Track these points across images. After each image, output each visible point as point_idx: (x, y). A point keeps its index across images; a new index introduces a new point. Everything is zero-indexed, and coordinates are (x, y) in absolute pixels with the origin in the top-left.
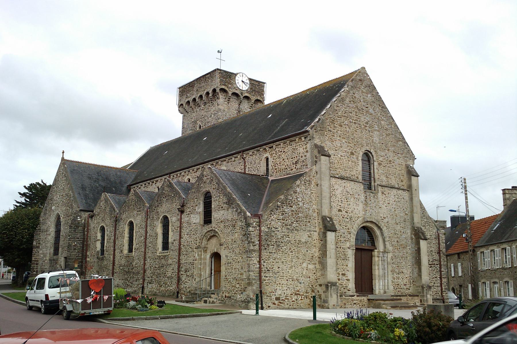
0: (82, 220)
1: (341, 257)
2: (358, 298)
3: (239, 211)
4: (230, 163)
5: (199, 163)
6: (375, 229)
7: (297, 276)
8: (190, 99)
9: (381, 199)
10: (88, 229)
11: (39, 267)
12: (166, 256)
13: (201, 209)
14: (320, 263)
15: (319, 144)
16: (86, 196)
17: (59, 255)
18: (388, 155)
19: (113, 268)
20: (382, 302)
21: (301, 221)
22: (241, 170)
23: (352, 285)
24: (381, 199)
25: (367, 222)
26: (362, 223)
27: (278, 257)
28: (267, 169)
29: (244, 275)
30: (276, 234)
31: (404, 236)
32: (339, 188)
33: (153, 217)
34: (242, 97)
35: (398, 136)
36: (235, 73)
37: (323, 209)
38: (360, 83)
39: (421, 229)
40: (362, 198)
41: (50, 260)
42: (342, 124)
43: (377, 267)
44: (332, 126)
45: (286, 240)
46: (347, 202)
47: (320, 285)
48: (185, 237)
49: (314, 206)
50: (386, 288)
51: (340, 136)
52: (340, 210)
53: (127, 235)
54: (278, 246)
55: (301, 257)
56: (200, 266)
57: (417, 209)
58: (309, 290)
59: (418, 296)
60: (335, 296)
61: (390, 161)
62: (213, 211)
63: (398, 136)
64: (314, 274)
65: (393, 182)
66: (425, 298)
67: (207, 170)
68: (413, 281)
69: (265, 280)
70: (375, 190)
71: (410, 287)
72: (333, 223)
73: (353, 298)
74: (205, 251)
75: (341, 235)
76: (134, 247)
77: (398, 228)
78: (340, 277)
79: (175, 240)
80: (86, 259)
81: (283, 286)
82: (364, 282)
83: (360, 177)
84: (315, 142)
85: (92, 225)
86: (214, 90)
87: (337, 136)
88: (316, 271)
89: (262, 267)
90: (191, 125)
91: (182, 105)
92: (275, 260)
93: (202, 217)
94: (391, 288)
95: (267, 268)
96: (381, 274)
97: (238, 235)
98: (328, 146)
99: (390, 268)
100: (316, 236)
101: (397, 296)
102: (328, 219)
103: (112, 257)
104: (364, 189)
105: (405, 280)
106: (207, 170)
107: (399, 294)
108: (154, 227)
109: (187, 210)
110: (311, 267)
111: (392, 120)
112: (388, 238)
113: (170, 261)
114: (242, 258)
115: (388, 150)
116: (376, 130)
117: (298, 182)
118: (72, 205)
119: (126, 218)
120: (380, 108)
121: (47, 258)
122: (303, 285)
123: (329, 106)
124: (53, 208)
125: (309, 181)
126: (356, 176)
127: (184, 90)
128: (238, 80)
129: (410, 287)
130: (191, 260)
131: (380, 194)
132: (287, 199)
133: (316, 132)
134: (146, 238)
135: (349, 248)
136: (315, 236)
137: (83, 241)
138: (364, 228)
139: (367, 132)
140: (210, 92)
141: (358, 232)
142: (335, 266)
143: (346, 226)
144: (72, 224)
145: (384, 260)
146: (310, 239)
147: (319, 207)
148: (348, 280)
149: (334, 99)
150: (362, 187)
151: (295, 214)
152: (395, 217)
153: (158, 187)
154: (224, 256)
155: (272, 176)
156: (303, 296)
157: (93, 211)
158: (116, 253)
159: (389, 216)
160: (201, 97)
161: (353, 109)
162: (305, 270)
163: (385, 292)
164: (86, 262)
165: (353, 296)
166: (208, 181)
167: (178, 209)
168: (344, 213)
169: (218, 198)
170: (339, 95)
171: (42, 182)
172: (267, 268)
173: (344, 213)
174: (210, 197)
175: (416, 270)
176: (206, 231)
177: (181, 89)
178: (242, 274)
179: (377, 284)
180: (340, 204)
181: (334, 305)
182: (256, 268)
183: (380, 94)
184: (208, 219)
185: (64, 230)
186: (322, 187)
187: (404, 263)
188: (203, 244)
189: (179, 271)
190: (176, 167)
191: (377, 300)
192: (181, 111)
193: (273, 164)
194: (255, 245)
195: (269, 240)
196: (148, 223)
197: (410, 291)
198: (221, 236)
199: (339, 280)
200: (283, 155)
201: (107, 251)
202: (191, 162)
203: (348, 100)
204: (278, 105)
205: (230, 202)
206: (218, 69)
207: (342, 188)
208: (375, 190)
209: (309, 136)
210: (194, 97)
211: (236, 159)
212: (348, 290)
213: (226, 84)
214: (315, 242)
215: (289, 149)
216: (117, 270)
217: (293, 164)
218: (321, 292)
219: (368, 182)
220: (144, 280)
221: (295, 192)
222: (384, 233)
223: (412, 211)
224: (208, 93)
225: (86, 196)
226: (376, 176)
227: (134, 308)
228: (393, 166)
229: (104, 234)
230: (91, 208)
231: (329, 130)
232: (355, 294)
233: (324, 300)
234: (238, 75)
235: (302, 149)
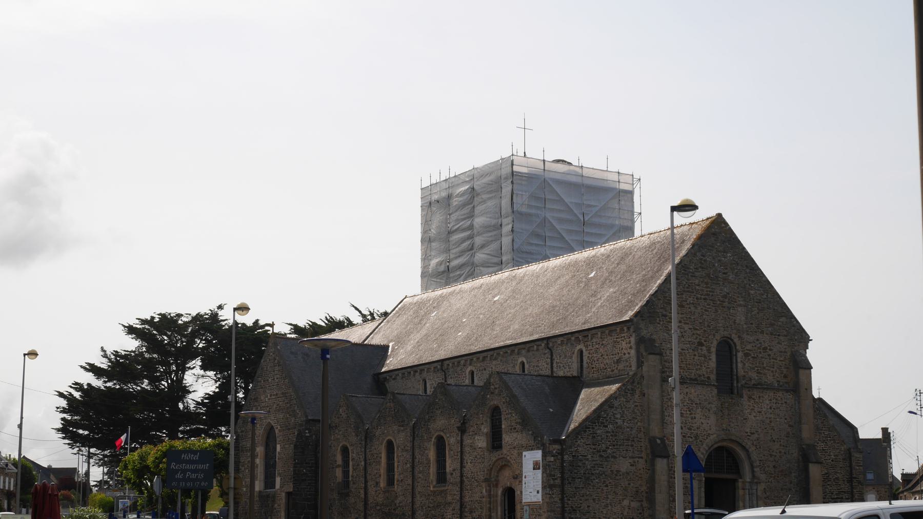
4: (531, 353)
13: (486, 429)
28: (582, 366)
42: (684, 303)
48: (468, 466)
49: (639, 424)
61: (765, 349)
74: (497, 486)
79: (454, 470)
83: (713, 377)
100: (641, 464)
103: (362, 492)
113: (449, 498)
116: (740, 305)
125: (632, 390)
134: (413, 467)
138: (720, 449)
150: (715, 391)
159: (759, 430)
162: (627, 510)
166: (497, 391)
176: (495, 459)
184: (496, 442)
196: (416, 443)
228: (769, 355)
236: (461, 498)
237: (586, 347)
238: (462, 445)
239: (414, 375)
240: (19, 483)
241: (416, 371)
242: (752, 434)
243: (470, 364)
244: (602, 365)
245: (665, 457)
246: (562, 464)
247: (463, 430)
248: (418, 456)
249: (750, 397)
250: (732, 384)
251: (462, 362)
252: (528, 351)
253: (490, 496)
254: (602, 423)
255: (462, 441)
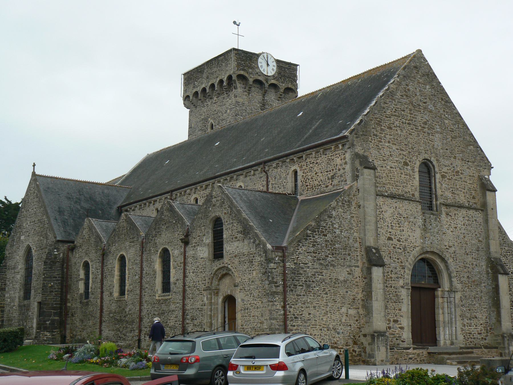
0: (59, 254)
1: (391, 298)
2: (415, 351)
3: (257, 242)
4: (248, 178)
5: (209, 177)
6: (438, 261)
7: (334, 324)
8: (199, 89)
9: (445, 222)
10: (68, 265)
11: (5, 316)
12: (167, 300)
13: (208, 239)
14: (364, 306)
15: (361, 152)
16: (64, 222)
17: (32, 298)
18: (454, 165)
19: (101, 316)
20: (447, 356)
21: (338, 254)
22: (263, 186)
23: (407, 335)
24: (445, 222)
25: (427, 252)
26: (421, 255)
27: (309, 300)
28: (296, 186)
29: (265, 324)
30: (305, 271)
31: (477, 270)
32: (388, 209)
33: (150, 250)
34: (267, 85)
35: (468, 138)
36: (257, 53)
37: (367, 237)
38: (415, 71)
39: (501, 261)
40: (420, 221)
41: (20, 306)
43: (441, 311)
44: (379, 129)
45: (318, 279)
46: (400, 227)
47: (365, 336)
48: (191, 275)
49: (355, 234)
50: (454, 337)
51: (389, 142)
52: (390, 239)
53: (117, 273)
54: (308, 286)
55: (338, 299)
56: (209, 313)
57: (494, 234)
58: (350, 342)
59: (497, 348)
60: (383, 349)
61: (457, 172)
62: (224, 242)
63: (468, 138)
64: (357, 321)
65: (462, 199)
66: (507, 351)
67: (216, 189)
68: (491, 329)
69: (292, 330)
70: (437, 211)
71: (487, 336)
72: (380, 255)
73: (408, 351)
75: (392, 271)
76: (126, 288)
77: (469, 259)
78: (391, 325)
79: (177, 280)
80: (66, 304)
81: (316, 337)
82: (425, 331)
83: (417, 194)
84: (356, 150)
85: (73, 260)
86: (230, 78)
87: (385, 142)
88: (360, 317)
89: (288, 313)
90: (200, 124)
91: (188, 97)
92: (304, 304)
93: (212, 249)
94: (461, 337)
95: (294, 315)
96: (447, 319)
97: (256, 274)
98: (373, 156)
99: (459, 313)
100: (358, 272)
101: (468, 348)
102: (374, 251)
103: (99, 301)
104: (422, 209)
105: (480, 328)
106: (216, 189)
107: (472, 346)
108: (151, 263)
109: (193, 241)
110: (352, 312)
111: (458, 118)
112: (455, 273)
113: (172, 307)
114: (262, 302)
115: (455, 158)
116: (437, 132)
117: (334, 204)
118: (46, 234)
119: (117, 250)
120: (443, 103)
121: (16, 304)
122: (342, 335)
123: (373, 103)
124: (22, 238)
125: (349, 201)
126: (411, 193)
127: (190, 77)
128: (261, 63)
129: (487, 336)
130: (198, 305)
131: (444, 216)
132: (319, 226)
133: (357, 137)
134: (141, 278)
135: (402, 287)
136: (357, 273)
137: (62, 281)
138: (423, 260)
139: (426, 134)
140: (225, 79)
141: (414, 266)
142: (383, 310)
143: (398, 259)
144: (46, 259)
145: (450, 302)
146: (351, 276)
147: (362, 235)
148: (402, 328)
149: (381, 94)
150: (420, 207)
151: (331, 244)
152: (464, 245)
153: (157, 209)
154: (240, 300)
155: (301, 194)
156: (342, 350)
157: (73, 242)
158: (104, 297)
159: (456, 244)
160: (213, 86)
161: (406, 106)
163: (452, 343)
164: (66, 307)
165: (408, 349)
167: (181, 240)
168: (395, 241)
169: (231, 226)
170: (387, 88)
171: (6, 199)
172: (294, 315)
173: (395, 241)
174: (221, 224)
175: (494, 315)
176: (216, 268)
177: (186, 76)
178: (262, 323)
179: (442, 333)
180: (391, 230)
181: (382, 361)
182: (280, 315)
183: (443, 84)
184: (218, 252)
185: (37, 267)
186: (366, 209)
187: (477, 305)
188: (213, 285)
189: (184, 319)
190: (180, 183)
191: (440, 353)
192: (187, 104)
193: (303, 180)
194: (278, 286)
195: (297, 278)
196: (145, 257)
197: (487, 341)
198: (236, 274)
199: (390, 328)
200: (315, 168)
201: (92, 294)
202: (199, 176)
203: (399, 94)
204: (312, 97)
205: (246, 231)
206: (234, 49)
207: (392, 210)
208: (437, 211)
209: (347, 143)
210: (203, 86)
211: (257, 172)
212: (403, 341)
213: (246, 68)
214: (357, 280)
215: (323, 159)
216: (105, 318)
217: (329, 179)
218: (366, 344)
219: (429, 202)
220: (140, 331)
221: (330, 217)
222: (450, 266)
223: (487, 237)
224: (221, 81)
225: (64, 222)
226: (439, 192)
227: (126, 366)
228: (461, 178)
229: (89, 272)
230: (71, 238)
231: (374, 135)
232: (412, 346)
233: (369, 354)
234: (261, 56)
235: (341, 160)
236: (184, 305)
237: (301, 167)
238: (185, 256)
239: (149, 206)
240: (227, 315)
241: (150, 203)
242: (450, 247)
243: (195, 193)
244: (316, 183)
245: (381, 266)
246: (284, 271)
247: (186, 242)
248: (146, 269)
249: (447, 214)
250: (431, 202)
251: (188, 191)
252: (246, 176)
253: (211, 304)
254: (322, 232)
255: (185, 252)
